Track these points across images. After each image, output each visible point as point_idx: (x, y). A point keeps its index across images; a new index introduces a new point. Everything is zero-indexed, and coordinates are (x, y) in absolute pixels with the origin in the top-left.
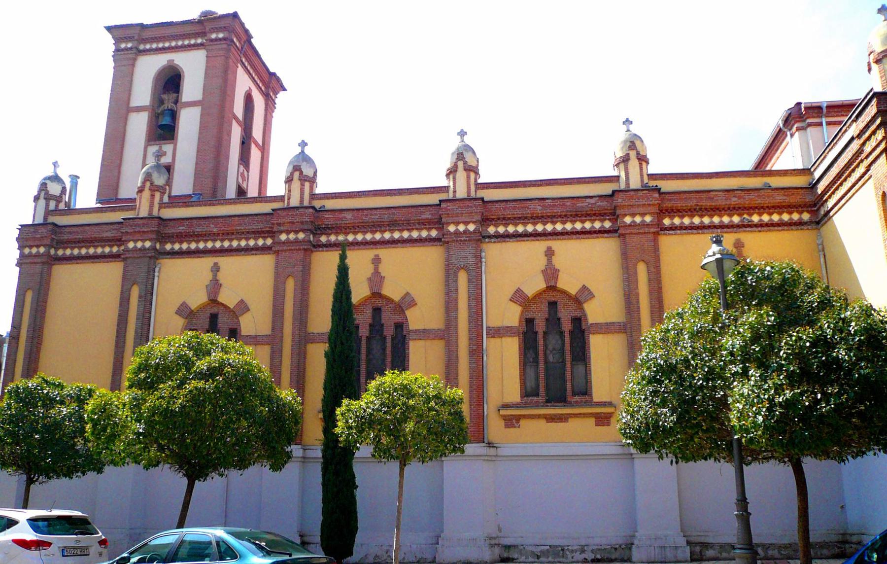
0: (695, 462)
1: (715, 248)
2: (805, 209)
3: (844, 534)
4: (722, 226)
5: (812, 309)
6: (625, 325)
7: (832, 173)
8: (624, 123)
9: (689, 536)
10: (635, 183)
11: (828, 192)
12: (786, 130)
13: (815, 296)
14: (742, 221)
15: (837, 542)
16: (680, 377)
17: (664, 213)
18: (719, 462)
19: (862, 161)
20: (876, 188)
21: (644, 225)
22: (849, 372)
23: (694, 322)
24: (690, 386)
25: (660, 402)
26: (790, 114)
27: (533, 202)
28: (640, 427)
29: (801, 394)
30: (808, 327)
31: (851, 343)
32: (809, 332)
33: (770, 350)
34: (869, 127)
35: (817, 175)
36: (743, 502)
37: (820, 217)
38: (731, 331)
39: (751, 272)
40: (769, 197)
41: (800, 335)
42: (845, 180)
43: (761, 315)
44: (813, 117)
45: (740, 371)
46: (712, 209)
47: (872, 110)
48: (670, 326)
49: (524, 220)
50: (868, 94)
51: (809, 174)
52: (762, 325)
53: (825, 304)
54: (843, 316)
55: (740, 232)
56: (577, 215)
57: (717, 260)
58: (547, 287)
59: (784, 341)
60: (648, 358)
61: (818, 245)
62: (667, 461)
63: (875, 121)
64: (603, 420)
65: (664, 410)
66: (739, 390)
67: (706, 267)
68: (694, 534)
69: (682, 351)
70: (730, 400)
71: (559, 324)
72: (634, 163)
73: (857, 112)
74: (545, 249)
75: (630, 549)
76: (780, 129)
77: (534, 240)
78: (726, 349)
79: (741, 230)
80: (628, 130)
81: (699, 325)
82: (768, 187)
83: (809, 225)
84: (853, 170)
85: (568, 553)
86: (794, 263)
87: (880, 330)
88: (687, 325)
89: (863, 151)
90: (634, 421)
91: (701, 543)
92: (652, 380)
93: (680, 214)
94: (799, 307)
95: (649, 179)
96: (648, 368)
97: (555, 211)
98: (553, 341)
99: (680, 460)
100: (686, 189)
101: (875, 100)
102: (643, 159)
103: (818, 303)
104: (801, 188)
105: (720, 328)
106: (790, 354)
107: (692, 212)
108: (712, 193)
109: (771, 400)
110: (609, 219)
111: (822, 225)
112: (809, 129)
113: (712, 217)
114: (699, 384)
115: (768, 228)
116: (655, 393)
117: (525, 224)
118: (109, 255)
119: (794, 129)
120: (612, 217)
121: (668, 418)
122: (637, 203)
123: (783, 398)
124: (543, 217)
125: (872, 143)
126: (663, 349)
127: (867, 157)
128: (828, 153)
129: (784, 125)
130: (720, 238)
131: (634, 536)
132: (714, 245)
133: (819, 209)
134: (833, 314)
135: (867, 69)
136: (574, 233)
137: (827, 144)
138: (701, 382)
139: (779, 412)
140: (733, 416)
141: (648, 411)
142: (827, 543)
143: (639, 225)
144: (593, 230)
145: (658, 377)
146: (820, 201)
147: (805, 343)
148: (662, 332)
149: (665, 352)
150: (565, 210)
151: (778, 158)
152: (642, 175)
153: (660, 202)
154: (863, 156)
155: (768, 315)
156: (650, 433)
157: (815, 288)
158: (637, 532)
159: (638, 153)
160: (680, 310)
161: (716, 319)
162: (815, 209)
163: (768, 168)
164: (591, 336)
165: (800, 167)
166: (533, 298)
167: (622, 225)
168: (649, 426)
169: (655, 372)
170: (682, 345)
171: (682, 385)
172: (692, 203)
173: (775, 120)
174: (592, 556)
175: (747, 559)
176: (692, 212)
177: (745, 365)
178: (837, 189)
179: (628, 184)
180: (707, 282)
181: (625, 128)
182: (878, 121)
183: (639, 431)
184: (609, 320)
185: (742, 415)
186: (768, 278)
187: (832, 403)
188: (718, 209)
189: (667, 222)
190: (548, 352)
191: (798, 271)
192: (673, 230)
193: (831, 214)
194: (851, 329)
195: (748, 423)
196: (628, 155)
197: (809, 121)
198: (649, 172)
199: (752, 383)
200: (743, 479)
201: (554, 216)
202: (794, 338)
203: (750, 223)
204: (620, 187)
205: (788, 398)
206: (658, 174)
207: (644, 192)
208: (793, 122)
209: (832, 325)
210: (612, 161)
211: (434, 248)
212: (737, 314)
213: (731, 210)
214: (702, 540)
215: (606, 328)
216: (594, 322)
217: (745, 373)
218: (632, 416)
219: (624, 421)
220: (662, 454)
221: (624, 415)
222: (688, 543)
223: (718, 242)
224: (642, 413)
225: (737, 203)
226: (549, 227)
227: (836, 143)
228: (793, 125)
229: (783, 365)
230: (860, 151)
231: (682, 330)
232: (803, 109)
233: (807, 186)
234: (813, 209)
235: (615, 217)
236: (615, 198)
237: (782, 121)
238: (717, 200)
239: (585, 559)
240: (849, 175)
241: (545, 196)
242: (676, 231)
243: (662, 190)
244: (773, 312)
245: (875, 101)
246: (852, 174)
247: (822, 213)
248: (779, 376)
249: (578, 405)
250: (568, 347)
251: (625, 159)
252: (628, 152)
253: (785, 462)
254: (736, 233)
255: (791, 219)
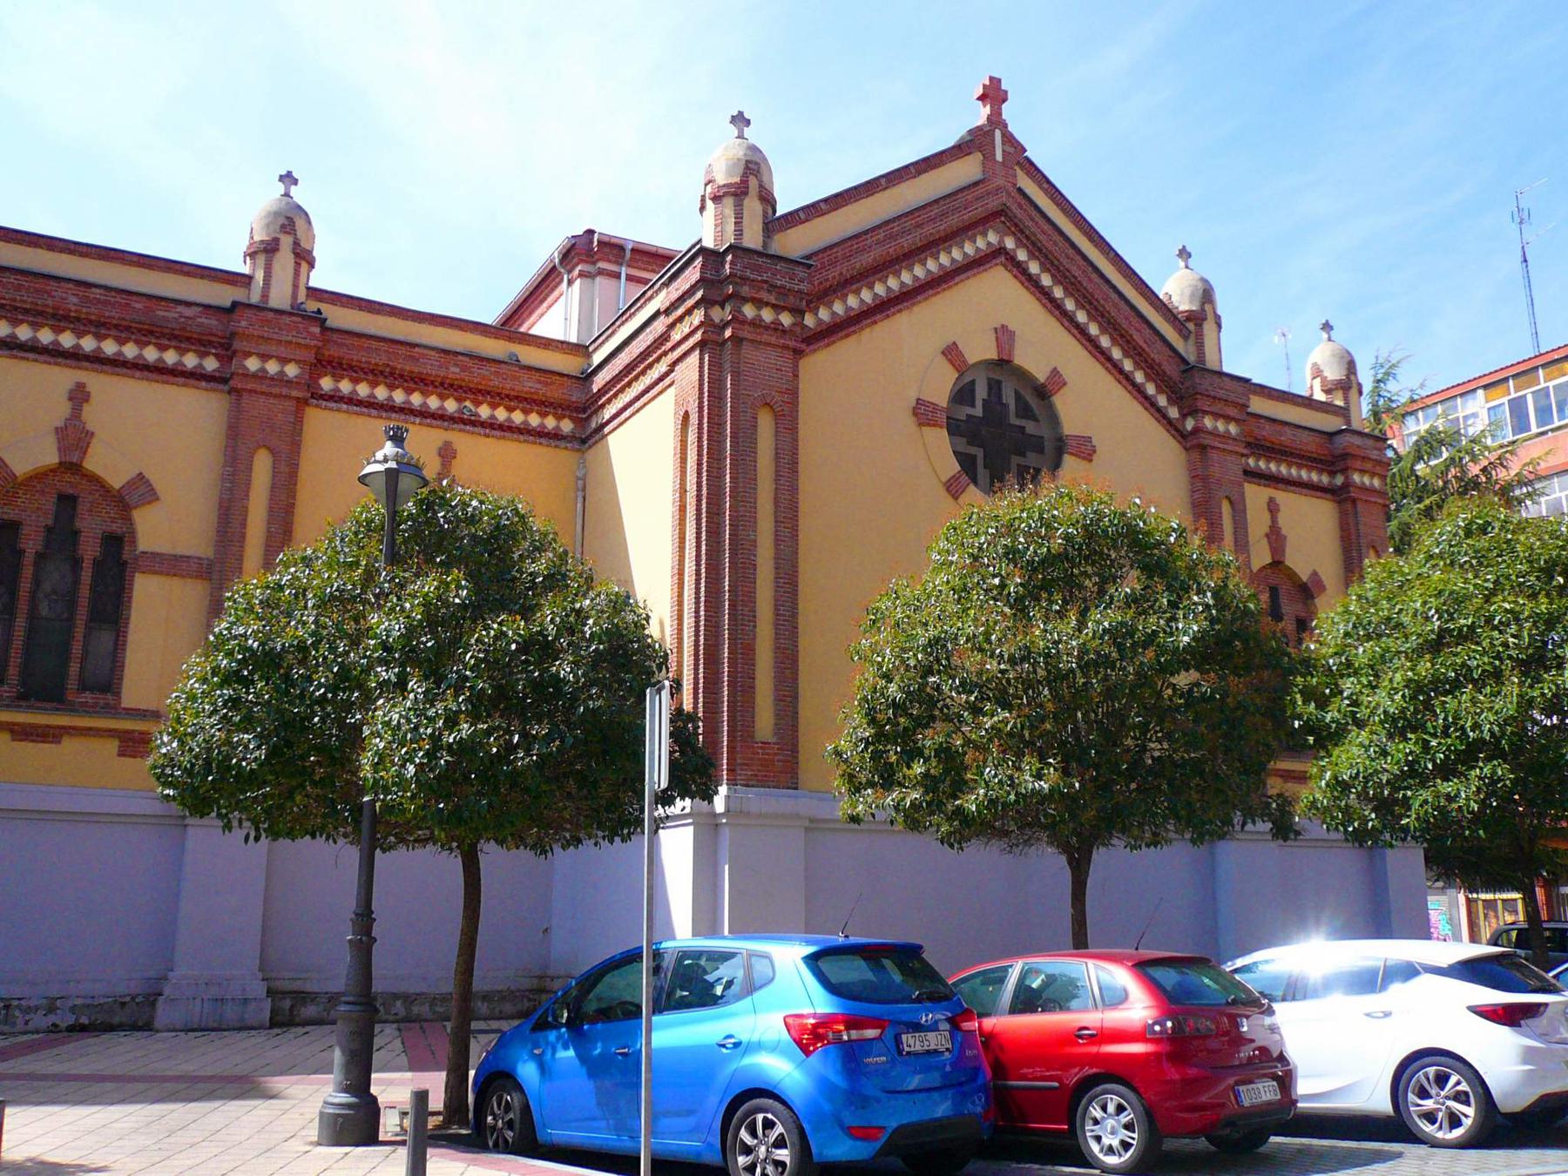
0: (293, 840)
1: (389, 448)
2: (567, 413)
3: (540, 977)
4: (406, 410)
5: (534, 586)
6: (211, 564)
7: (619, 362)
8: (281, 178)
9: (275, 979)
10: (280, 297)
11: (606, 392)
12: (562, 270)
13: (542, 564)
14: (460, 411)
15: (531, 991)
16: (287, 678)
17: (324, 366)
18: (335, 842)
19: (665, 354)
20: (677, 403)
21: (281, 381)
22: (574, 699)
23: (329, 577)
24: (302, 696)
25: (240, 720)
26: (574, 245)
27: (62, 284)
28: (193, 765)
29: (488, 733)
30: (518, 617)
31: (582, 652)
32: (519, 625)
33: (447, 651)
34: (685, 301)
35: (597, 358)
36: (365, 917)
37: (588, 432)
38: (389, 604)
39: (444, 503)
40: (515, 378)
41: (505, 629)
42: (636, 378)
43: (448, 584)
44: (609, 261)
45: (394, 679)
46: (412, 379)
47: (692, 275)
48: (285, 579)
49: (34, 316)
50: (694, 246)
51: (584, 356)
52: (447, 604)
53: (556, 580)
54: (578, 606)
55: (453, 429)
56: (151, 332)
57: (387, 470)
58: (61, 463)
59: (476, 635)
60: (231, 633)
61: (578, 478)
62: (239, 834)
63: (694, 293)
64: (134, 745)
65: (246, 736)
66: (385, 715)
67: (367, 480)
68: (287, 975)
69: (297, 629)
70: (366, 731)
71: (75, 543)
72: (285, 259)
73: (673, 271)
74: (440, 444)
75: (153, 1004)
76: (554, 267)
77: (50, 363)
78: (375, 637)
79: (455, 426)
80: (287, 195)
81: (336, 585)
82: (515, 362)
83: (570, 442)
84: (650, 366)
85: (17, 1013)
86: (520, 502)
87: (631, 637)
88: (315, 582)
89: (669, 336)
90: (183, 752)
91: (295, 992)
92: (229, 678)
93: (354, 375)
94: (514, 579)
95: (307, 296)
96: (230, 654)
97: (107, 314)
98: (55, 574)
99: (264, 835)
100: (372, 331)
101: (700, 259)
102: (304, 258)
103: (545, 578)
104: (568, 376)
105: (377, 596)
106: (483, 660)
107: (375, 375)
108: (417, 349)
109: (435, 739)
110: (216, 355)
111: (590, 447)
112: (598, 279)
113: (428, 397)
114: (317, 694)
115: (502, 433)
116: (234, 703)
117: (36, 326)
118: (133, 364)
119: (576, 272)
120: (224, 352)
121: (251, 750)
122: (275, 336)
123: (455, 738)
124: (78, 319)
125: (684, 328)
126: (261, 620)
127: (673, 348)
128: (619, 327)
129: (561, 262)
130: (402, 433)
131: (165, 978)
132: (389, 444)
133: (589, 418)
134: (565, 600)
135: (699, 206)
136: (138, 367)
137: (621, 312)
138: (322, 690)
139: (445, 761)
140: (366, 760)
141: (213, 736)
142: (513, 992)
143: (272, 379)
144: (180, 368)
145: (246, 673)
146: (592, 405)
147: (509, 644)
148: (268, 587)
149: (264, 626)
150: (127, 317)
151: (542, 315)
152: (296, 286)
153: (320, 344)
154: (669, 345)
155: (459, 587)
156: (210, 778)
157: (545, 551)
158: (172, 970)
159: (296, 244)
160: (309, 551)
161: (369, 577)
162: (584, 416)
163: (522, 330)
164: (137, 575)
165: (573, 339)
166: (26, 479)
167: (240, 371)
168: (210, 764)
169: (239, 662)
170: (299, 617)
171: (287, 693)
172: (379, 359)
173: (546, 249)
174: (70, 1020)
175: (357, 1022)
176: (376, 375)
177: (405, 669)
178: (622, 390)
179: (265, 295)
180: (366, 508)
181: (281, 188)
182: (699, 294)
183: (189, 772)
184: (179, 551)
185: (381, 761)
186: (472, 520)
187: (535, 752)
188: (422, 380)
189: (326, 383)
190: (41, 595)
191: (523, 517)
192: (336, 402)
193: (607, 430)
194: (586, 629)
195: (387, 775)
196: (276, 240)
197: (602, 265)
198: (312, 283)
199: (409, 704)
200: (372, 876)
201: (104, 324)
202: (492, 633)
203: (473, 418)
204: (249, 298)
205: (464, 736)
206: (326, 292)
207: (294, 318)
208: (575, 260)
209: (558, 619)
210: (243, 244)
211: (213, 396)
212: (407, 575)
213: (446, 387)
214: (296, 986)
215: (171, 565)
216: (150, 550)
217: (401, 685)
218: (182, 743)
219: (164, 751)
220: (229, 821)
221: (165, 739)
222: (270, 992)
223: (398, 439)
224: (200, 738)
225: (458, 377)
226: (46, 336)
227: (634, 314)
228: (577, 264)
229: (466, 678)
230: (664, 337)
231: (305, 590)
232: (596, 243)
233: (578, 375)
234: (580, 416)
235: (229, 353)
236: (235, 316)
237: (559, 253)
238: (425, 364)
239: (54, 1025)
240: (643, 373)
241: (91, 278)
242: (339, 405)
243: (327, 322)
244: (467, 581)
245: (699, 262)
246: (648, 371)
247: (593, 425)
248: (456, 696)
249: (87, 712)
250: (85, 592)
251: (269, 247)
252: (278, 236)
253: (451, 849)
254: (446, 430)
255: (509, 420)
